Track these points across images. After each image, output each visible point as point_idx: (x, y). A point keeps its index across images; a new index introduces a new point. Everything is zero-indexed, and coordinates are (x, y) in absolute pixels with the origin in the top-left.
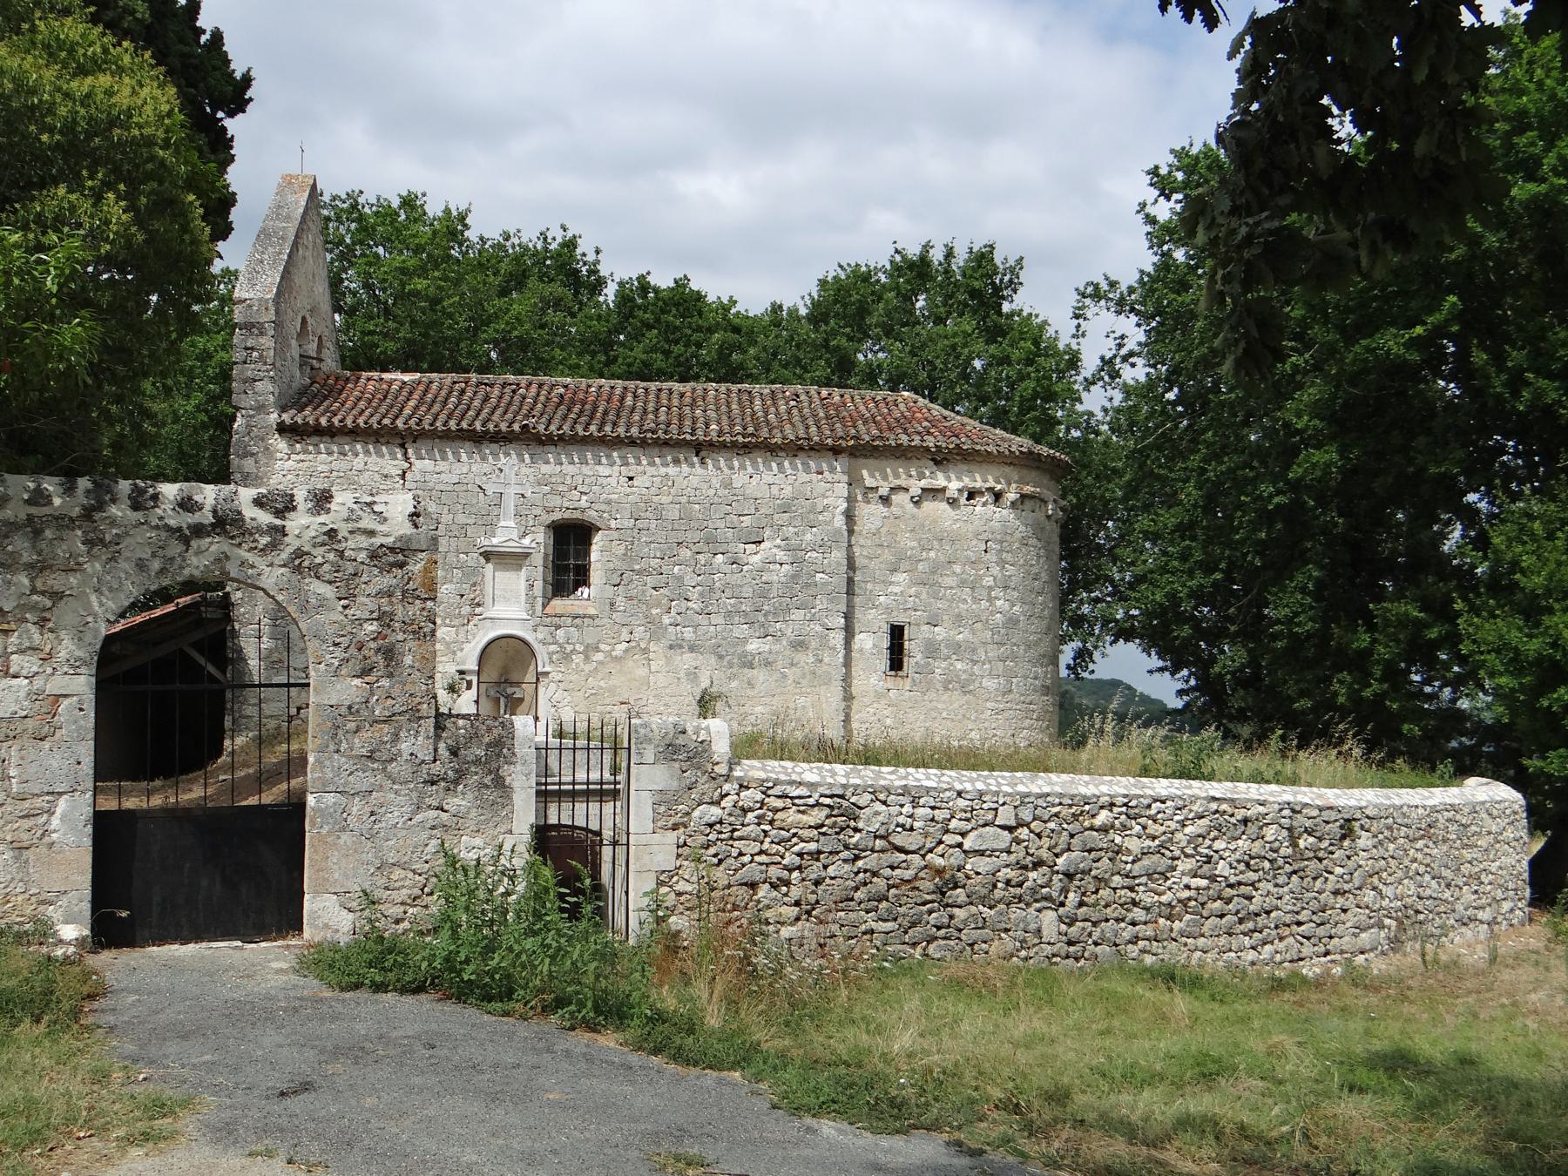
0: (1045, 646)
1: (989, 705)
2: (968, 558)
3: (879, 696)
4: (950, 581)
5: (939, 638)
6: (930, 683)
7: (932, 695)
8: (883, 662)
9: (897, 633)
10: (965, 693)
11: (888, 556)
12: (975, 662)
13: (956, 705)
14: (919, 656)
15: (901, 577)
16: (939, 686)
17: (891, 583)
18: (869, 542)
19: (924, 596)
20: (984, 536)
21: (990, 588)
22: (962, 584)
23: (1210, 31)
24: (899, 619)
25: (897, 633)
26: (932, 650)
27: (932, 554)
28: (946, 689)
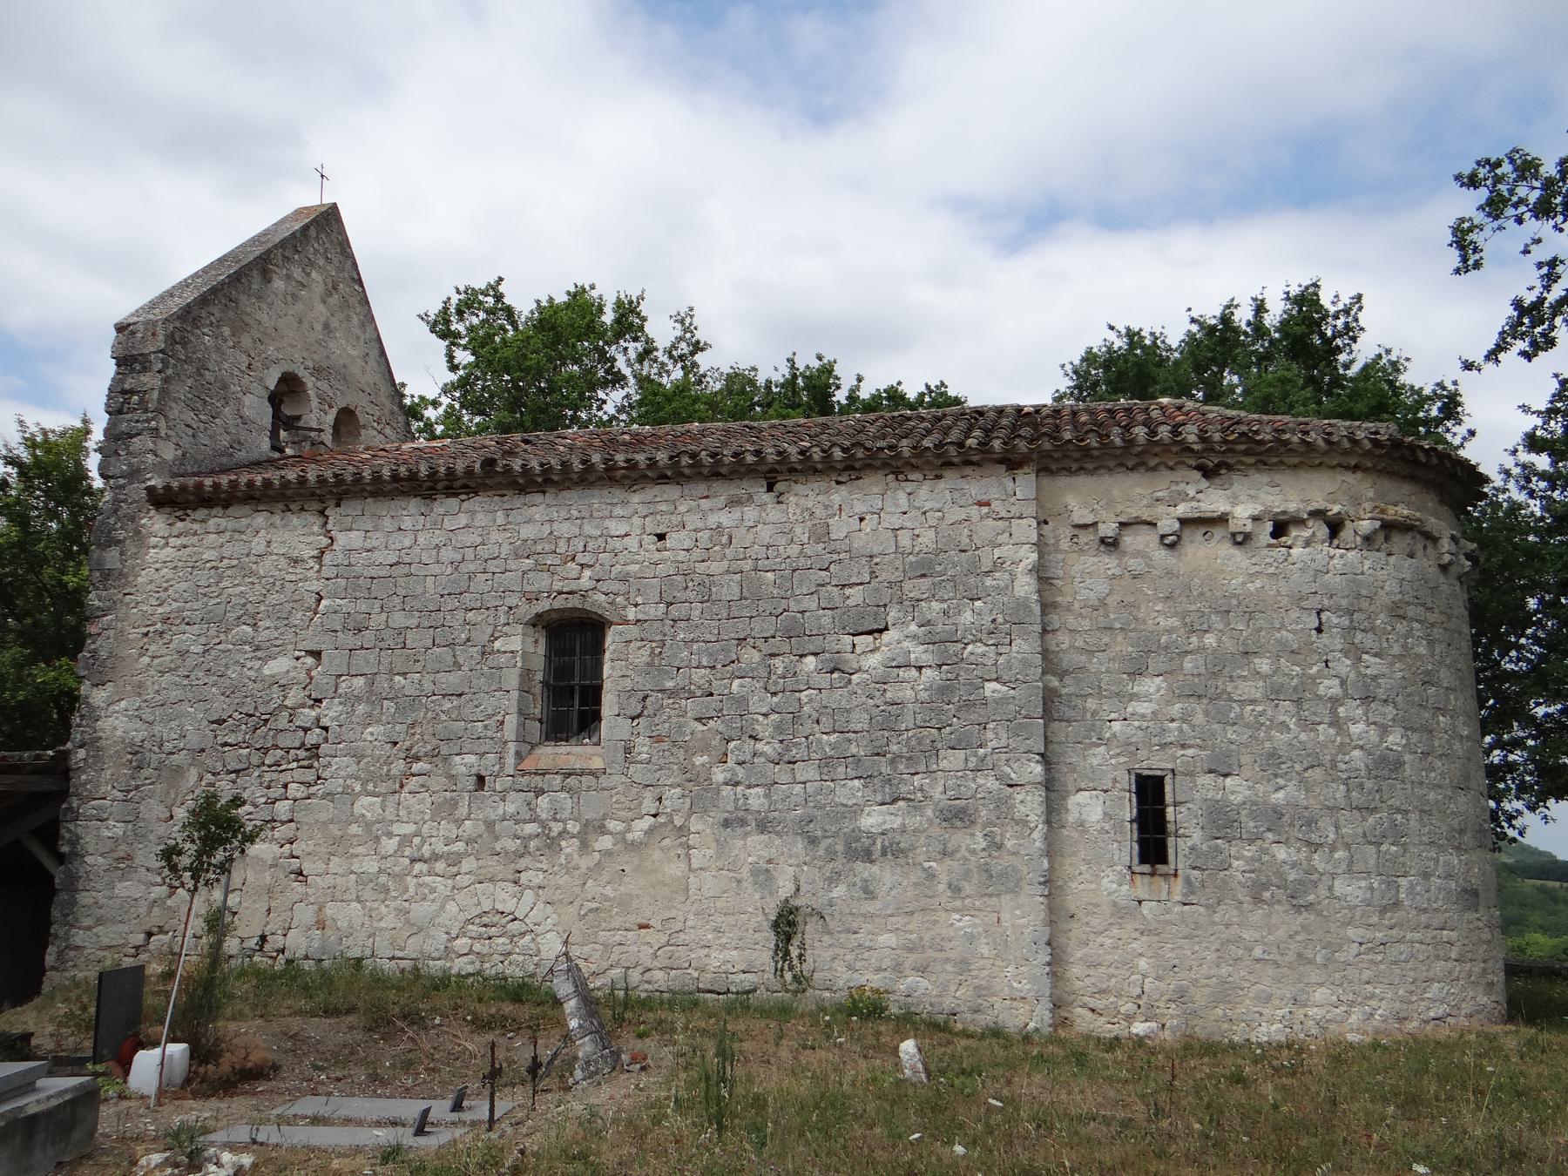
1: (1351, 932)
2: (1282, 644)
3: (1120, 912)
7: (1227, 912)
8: (1125, 847)
10: (1298, 908)
11: (1122, 646)
12: (1314, 847)
13: (1281, 933)
14: (1197, 836)
15: (1151, 685)
17: (1133, 697)
18: (1086, 624)
20: (1314, 602)
21: (1335, 701)
22: (1275, 694)
24: (1154, 763)
26: (1222, 822)
27: (1210, 640)
28: (1257, 900)
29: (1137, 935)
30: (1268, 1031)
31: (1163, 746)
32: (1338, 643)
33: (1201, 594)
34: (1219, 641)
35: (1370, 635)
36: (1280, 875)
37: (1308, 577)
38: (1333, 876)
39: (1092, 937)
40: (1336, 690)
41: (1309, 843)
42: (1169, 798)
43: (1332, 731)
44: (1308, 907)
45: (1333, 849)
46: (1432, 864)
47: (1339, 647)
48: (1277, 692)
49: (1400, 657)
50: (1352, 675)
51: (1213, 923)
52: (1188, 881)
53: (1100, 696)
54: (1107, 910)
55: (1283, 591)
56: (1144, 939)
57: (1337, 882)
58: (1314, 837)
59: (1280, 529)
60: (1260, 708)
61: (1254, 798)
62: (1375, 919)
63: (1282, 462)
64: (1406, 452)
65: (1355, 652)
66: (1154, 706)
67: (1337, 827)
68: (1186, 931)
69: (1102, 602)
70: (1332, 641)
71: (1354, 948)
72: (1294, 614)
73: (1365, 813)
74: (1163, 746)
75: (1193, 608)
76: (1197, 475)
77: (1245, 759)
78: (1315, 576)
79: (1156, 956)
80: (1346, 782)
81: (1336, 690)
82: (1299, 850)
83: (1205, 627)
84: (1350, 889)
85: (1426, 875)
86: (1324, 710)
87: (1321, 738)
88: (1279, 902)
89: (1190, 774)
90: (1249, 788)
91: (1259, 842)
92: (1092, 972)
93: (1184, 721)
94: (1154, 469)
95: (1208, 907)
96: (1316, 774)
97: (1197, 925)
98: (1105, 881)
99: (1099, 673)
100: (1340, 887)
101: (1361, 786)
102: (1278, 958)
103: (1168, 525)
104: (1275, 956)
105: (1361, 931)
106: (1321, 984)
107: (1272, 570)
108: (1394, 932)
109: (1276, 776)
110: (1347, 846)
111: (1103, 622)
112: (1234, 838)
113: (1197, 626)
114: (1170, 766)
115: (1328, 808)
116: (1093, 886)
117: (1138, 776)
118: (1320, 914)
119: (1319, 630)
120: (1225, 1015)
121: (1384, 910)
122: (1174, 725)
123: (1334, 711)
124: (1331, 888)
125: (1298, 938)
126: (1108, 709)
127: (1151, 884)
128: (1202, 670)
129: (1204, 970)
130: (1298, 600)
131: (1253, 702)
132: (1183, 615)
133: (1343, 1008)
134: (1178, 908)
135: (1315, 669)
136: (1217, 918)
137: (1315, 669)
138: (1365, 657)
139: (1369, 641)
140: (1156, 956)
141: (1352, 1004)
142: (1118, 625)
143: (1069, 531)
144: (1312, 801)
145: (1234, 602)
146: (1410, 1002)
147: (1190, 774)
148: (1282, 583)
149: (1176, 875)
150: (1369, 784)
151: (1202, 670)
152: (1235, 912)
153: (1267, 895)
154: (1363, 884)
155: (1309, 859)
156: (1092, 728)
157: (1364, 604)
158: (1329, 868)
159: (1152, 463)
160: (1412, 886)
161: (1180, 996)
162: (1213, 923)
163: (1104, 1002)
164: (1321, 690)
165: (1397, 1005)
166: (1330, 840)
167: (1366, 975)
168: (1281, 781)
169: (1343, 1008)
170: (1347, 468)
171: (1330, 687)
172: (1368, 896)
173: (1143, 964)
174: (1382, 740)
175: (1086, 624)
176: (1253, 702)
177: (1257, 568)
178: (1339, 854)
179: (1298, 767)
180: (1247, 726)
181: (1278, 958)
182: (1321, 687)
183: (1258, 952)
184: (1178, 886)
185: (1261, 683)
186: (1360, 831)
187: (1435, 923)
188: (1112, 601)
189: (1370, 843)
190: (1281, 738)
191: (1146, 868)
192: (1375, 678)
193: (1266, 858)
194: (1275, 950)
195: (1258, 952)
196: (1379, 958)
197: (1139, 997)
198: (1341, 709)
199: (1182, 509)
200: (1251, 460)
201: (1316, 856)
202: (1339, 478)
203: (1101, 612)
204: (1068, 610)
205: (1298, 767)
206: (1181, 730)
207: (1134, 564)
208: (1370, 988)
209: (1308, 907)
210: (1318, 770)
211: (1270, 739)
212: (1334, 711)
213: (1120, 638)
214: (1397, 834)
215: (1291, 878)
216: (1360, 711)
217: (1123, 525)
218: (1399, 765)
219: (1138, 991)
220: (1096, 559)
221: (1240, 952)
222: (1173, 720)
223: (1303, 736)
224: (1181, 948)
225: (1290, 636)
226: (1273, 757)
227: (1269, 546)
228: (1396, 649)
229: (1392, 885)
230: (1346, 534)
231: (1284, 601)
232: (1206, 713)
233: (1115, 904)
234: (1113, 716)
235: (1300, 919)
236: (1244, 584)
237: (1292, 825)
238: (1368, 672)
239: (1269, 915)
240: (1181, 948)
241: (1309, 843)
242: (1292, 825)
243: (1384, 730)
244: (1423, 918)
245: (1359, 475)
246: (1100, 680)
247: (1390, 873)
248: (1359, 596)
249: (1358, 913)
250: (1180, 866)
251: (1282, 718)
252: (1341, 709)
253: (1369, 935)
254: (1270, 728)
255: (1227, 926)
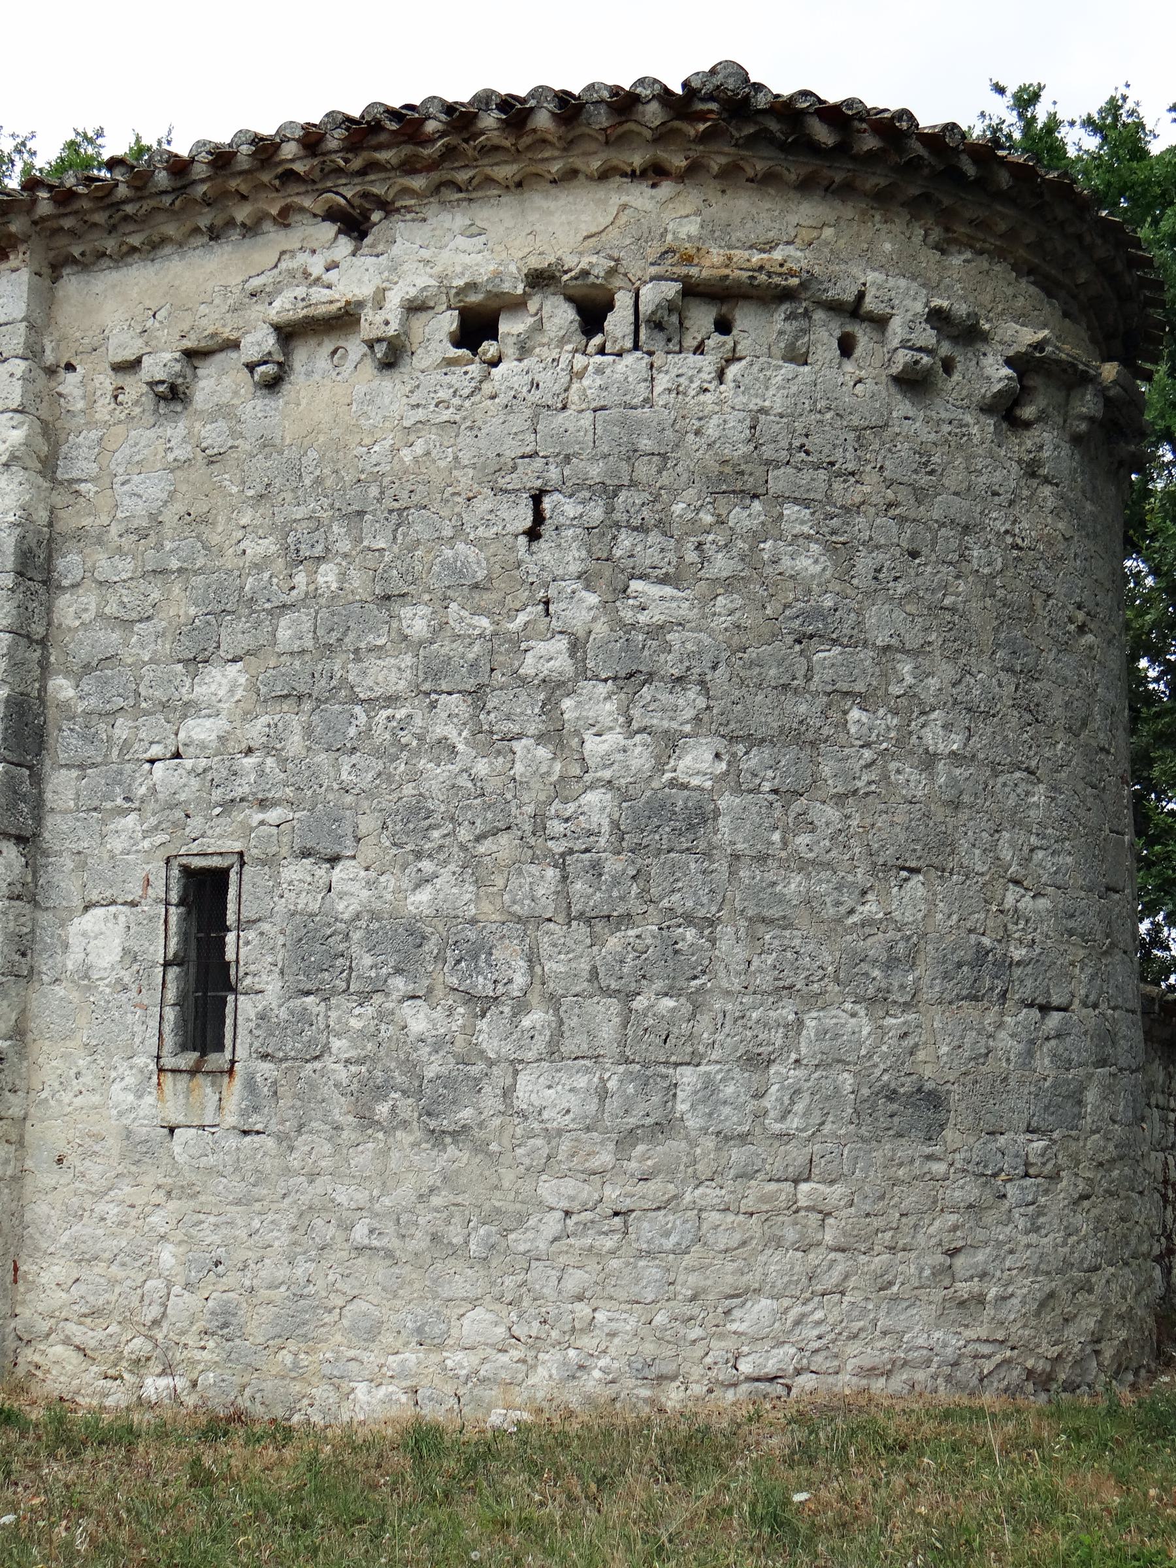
0: (53, 630)
1: (548, 1189)
2: (455, 570)
3: (138, 1150)
4: (388, 673)
5: (345, 908)
6: (308, 1095)
7: (315, 1147)
8: (146, 1019)
9: (204, 894)
10: (437, 1137)
11: (181, 606)
12: (480, 1004)
13: (405, 1193)
14: (272, 986)
15: (222, 682)
16: (341, 1111)
17: (189, 708)
18: (126, 568)
19: (295, 744)
20: (528, 476)
21: (554, 688)
22: (430, 684)
23: (1041, 88)
24: (215, 842)
25: (204, 894)
26: (318, 958)
27: (328, 576)
28: (366, 1121)
29: (159, 1197)
30: (372, 1401)
31: (229, 805)
32: (574, 559)
33: (318, 481)
34: (343, 576)
35: (654, 537)
36: (411, 1067)
37: (519, 422)
38: (515, 1065)
39: (88, 1202)
40: (562, 664)
41: (470, 998)
42: (231, 918)
43: (543, 752)
44: (460, 1133)
45: (521, 1007)
46: (778, 1037)
47: (574, 568)
48: (435, 674)
49: (729, 584)
50: (601, 629)
51: (287, 1171)
52: (251, 1085)
53: (137, 713)
54: (113, 1144)
55: (466, 458)
56: (172, 1205)
57: (522, 1079)
58: (482, 985)
59: (476, 328)
60: (401, 714)
61: (377, 905)
62: (605, 1158)
63: (489, 181)
64: (774, 126)
65: (611, 578)
66: (219, 725)
67: (532, 959)
68: (240, 1188)
69: (155, 519)
70: (561, 555)
71: (552, 1223)
72: (482, 506)
73: (599, 926)
74: (229, 805)
75: (300, 512)
76: (329, 229)
77: (368, 824)
78: (535, 419)
79: (188, 1240)
80: (561, 862)
81: (562, 664)
82: (450, 1012)
83: (318, 550)
84: (553, 1094)
85: (756, 1061)
86: (527, 712)
87: (519, 768)
88: (405, 1124)
89: (270, 861)
90: (370, 885)
91: (378, 999)
92: (84, 1272)
93: (268, 750)
94: (251, 230)
95: (281, 1138)
96: (503, 847)
97: (261, 1178)
98: (117, 1086)
99: (140, 664)
100: (530, 1088)
101: (596, 869)
102: (396, 1243)
103: (259, 342)
104: (389, 1241)
105: (570, 1186)
106: (475, 1302)
107: (446, 415)
108: (651, 1186)
109: (419, 855)
110: (553, 1001)
111: (151, 559)
112: (334, 992)
113: (305, 552)
114: (237, 846)
115: (519, 919)
116: (96, 1099)
117: (186, 870)
118: (480, 1148)
119: (533, 534)
120: (296, 1365)
121: (627, 1140)
122: (249, 762)
123: (550, 707)
124: (507, 1093)
125: (436, 1201)
126: (152, 734)
127: (189, 1091)
128: (309, 643)
129: (267, 1271)
130: (494, 476)
131: (391, 700)
132: (285, 529)
133: (515, 1354)
134: (233, 1141)
135: (522, 618)
136: (294, 1160)
137: (522, 618)
138: (636, 585)
139: (651, 550)
140: (188, 1240)
141: (536, 1343)
142: (175, 564)
143: (106, 381)
144: (486, 907)
145: (374, 491)
146: (677, 1341)
147: (270, 861)
148: (466, 438)
149: (231, 1072)
150: (613, 865)
151: (309, 643)
152: (327, 1148)
153: (382, 1110)
154: (582, 1082)
155: (470, 1031)
156: (116, 779)
157: (644, 470)
158: (507, 1049)
159: (242, 213)
160: (709, 1087)
161: (224, 1325)
162: (287, 1171)
163: (100, 1334)
164: (529, 666)
165: (649, 1348)
166: (515, 990)
167: (575, 1280)
168: (427, 866)
169: (515, 1354)
170: (633, 175)
171: (548, 656)
172: (592, 1107)
173: (167, 1256)
174: (659, 767)
175: (126, 568)
176: (391, 700)
177: (420, 414)
178: (536, 1017)
179: (464, 834)
180: (378, 752)
181: (396, 1243)
182: (530, 658)
183: (360, 1233)
184: (235, 1091)
185: (408, 660)
186: (584, 966)
187: (776, 1166)
188: (169, 517)
189: (606, 992)
190: (437, 775)
191: (188, 1059)
192: (657, 631)
193: (387, 1031)
194: (390, 1228)
195: (360, 1233)
196: (609, 1243)
197: (156, 1323)
198: (567, 703)
199: (284, 307)
200: (418, 183)
201: (483, 1024)
202: (616, 200)
203: (152, 540)
204: (100, 541)
205: (464, 834)
206: (261, 772)
207: (213, 434)
208: (583, 1310)
209: (460, 1133)
210: (504, 839)
211: (415, 777)
212: (550, 707)
213: (176, 590)
214: (684, 974)
215: (430, 1072)
216: (610, 706)
217: (192, 356)
218: (701, 817)
219: (154, 1312)
220: (151, 434)
221: (332, 1230)
222: (250, 751)
223: (482, 767)
224: (231, 1223)
225: (472, 553)
226: (417, 815)
227: (450, 362)
228: (721, 565)
229: (651, 1075)
230: (618, 322)
231: (465, 479)
232: (308, 731)
233: (128, 1134)
234: (155, 751)
235: (442, 1160)
236: (394, 450)
237: (440, 958)
238: (643, 618)
239: (385, 1152)
240: (231, 1223)
241: (470, 998)
242: (440, 958)
243: (671, 743)
244: (737, 1155)
245: (666, 189)
246: (138, 680)
247: (652, 1058)
248: (633, 454)
249: (565, 1145)
250: (241, 1053)
251: (439, 731)
252: (567, 703)
253: (587, 1192)
254: (417, 753)
255: (312, 1177)
